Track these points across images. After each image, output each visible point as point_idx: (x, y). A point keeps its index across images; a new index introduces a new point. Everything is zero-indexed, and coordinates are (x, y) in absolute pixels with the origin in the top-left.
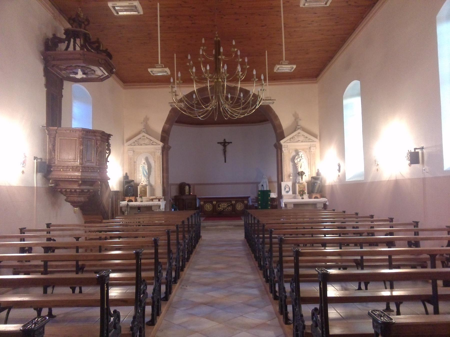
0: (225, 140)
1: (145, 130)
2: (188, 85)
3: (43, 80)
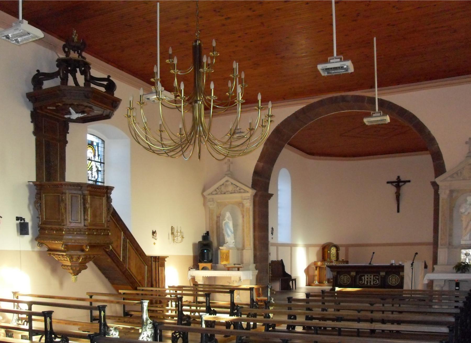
0: (399, 177)
1: (229, 172)
2: (286, 103)
3: (31, 127)
